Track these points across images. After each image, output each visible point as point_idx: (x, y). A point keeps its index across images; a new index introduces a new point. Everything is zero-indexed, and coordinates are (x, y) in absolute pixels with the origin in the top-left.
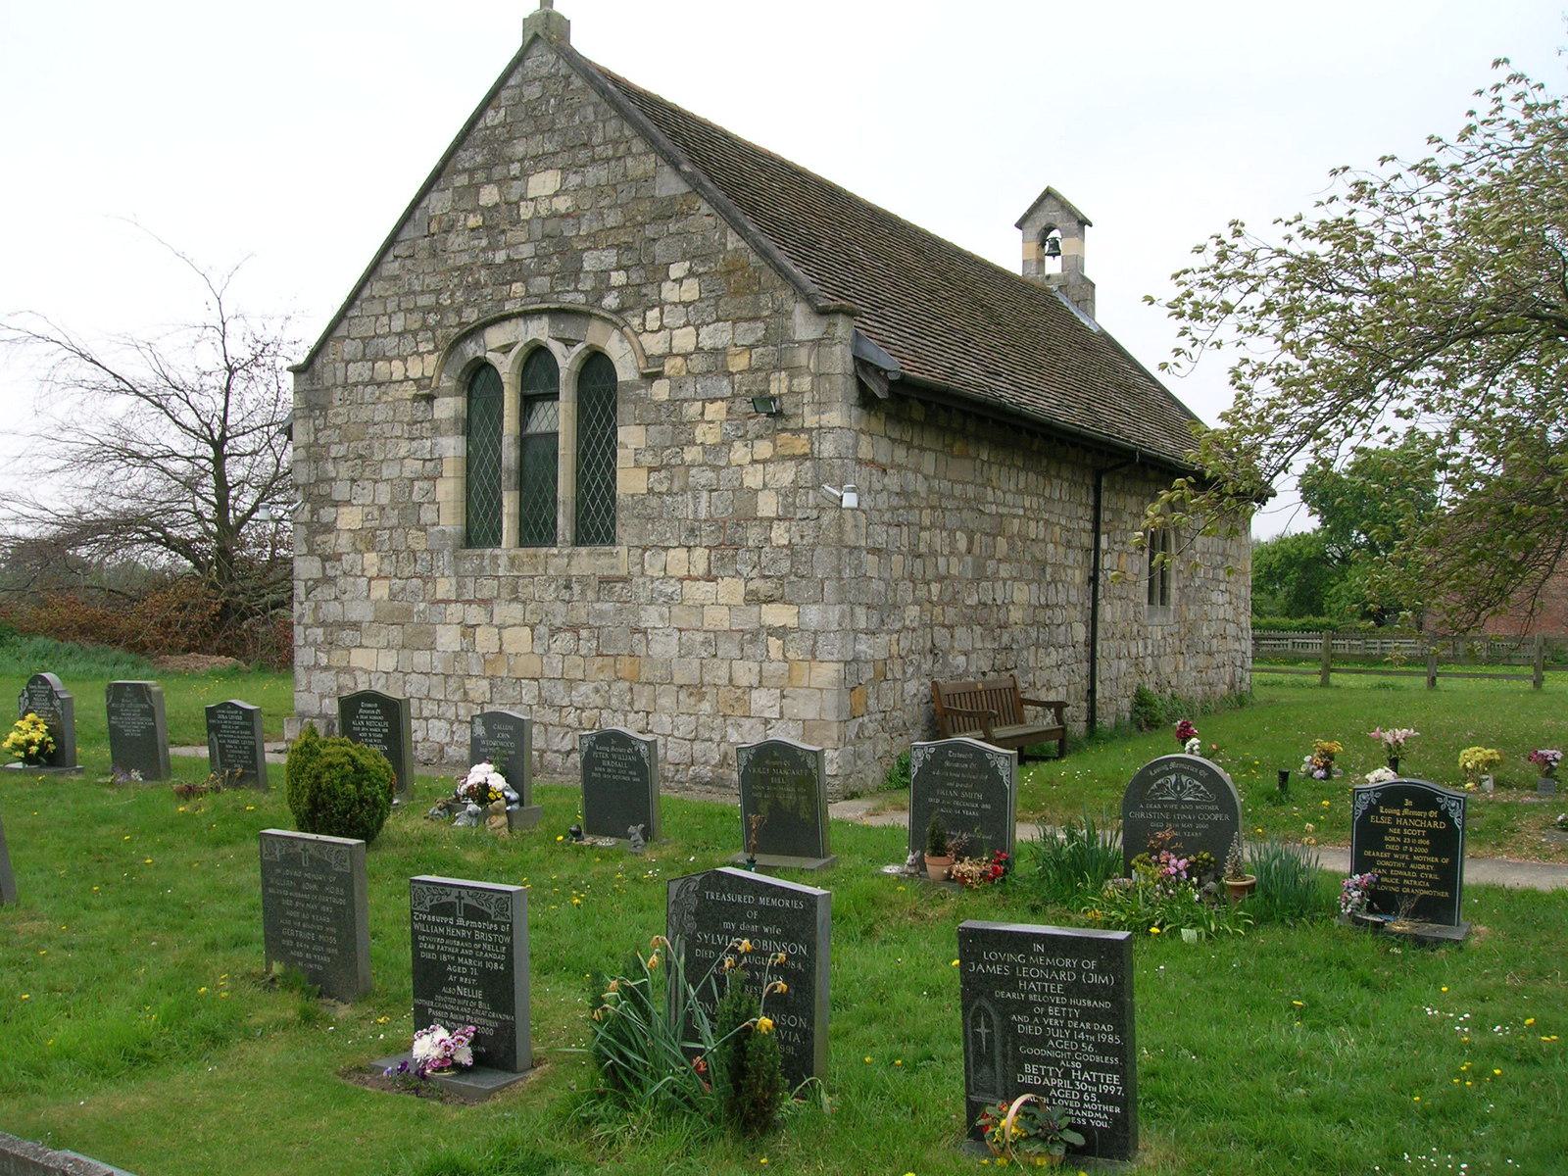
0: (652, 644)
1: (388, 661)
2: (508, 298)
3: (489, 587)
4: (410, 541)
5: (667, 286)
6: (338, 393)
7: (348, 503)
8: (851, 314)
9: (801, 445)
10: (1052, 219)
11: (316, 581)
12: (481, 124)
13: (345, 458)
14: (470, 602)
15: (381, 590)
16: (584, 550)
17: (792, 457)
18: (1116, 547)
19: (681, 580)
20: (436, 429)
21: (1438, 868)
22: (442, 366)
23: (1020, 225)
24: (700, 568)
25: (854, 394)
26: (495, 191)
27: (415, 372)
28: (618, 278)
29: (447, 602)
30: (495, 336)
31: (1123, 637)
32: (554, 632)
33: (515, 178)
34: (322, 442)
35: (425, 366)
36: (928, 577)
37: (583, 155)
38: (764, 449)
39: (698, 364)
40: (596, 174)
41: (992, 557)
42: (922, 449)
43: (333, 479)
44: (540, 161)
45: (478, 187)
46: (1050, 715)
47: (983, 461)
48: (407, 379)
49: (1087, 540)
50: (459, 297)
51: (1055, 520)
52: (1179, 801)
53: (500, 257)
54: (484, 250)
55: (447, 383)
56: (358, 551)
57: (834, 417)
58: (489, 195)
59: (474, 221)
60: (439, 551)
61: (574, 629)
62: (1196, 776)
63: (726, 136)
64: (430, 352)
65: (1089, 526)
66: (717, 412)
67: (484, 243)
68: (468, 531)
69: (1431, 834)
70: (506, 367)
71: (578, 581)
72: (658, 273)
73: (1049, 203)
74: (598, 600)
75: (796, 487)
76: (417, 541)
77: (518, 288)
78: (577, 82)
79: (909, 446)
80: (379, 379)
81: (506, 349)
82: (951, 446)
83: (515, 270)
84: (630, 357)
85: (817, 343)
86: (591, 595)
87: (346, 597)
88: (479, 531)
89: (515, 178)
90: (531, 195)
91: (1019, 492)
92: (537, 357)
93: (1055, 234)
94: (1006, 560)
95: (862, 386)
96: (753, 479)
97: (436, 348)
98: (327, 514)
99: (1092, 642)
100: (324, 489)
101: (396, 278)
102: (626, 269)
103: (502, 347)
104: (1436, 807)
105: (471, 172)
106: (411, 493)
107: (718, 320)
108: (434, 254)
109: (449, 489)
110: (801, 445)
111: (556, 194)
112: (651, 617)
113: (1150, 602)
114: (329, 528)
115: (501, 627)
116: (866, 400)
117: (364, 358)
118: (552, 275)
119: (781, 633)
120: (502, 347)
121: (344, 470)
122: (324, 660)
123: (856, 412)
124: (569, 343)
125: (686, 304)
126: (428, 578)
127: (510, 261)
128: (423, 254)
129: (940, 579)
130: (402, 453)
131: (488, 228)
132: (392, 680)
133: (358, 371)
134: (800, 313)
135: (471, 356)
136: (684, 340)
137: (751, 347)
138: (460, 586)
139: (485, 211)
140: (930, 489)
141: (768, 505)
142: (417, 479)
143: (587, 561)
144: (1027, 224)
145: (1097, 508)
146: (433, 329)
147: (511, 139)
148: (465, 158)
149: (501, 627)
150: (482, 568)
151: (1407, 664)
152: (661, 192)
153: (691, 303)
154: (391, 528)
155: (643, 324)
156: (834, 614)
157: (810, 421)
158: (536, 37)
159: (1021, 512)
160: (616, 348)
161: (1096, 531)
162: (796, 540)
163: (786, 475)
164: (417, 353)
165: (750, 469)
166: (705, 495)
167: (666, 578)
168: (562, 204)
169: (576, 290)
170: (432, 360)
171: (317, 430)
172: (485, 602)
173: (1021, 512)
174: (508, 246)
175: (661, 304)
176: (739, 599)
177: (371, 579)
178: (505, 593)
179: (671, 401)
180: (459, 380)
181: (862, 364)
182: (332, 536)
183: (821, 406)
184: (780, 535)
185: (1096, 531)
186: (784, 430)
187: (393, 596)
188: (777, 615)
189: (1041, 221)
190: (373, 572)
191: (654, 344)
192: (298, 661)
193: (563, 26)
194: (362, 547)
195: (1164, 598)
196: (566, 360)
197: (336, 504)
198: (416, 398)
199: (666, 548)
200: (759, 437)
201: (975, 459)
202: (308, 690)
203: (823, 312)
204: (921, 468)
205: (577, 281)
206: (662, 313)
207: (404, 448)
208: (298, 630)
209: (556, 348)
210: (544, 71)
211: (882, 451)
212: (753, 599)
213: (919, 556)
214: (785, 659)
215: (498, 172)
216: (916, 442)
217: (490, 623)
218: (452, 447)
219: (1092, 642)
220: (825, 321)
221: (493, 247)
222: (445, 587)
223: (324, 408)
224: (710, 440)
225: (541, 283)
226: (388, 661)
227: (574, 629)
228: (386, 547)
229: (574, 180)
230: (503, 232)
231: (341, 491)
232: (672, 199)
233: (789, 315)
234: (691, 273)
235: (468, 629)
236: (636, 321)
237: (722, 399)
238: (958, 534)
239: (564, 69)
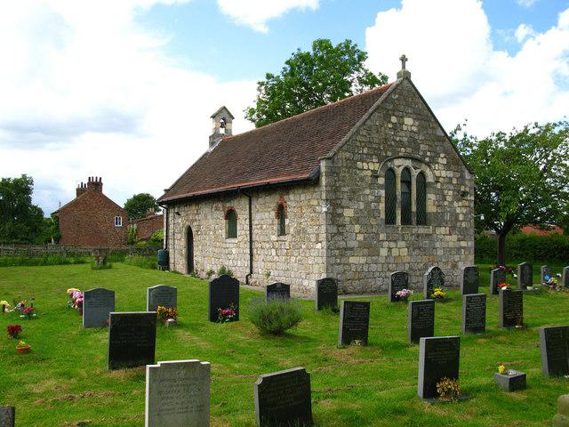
7: (348, 207)
15: (360, 237)
38: (460, 204)
70: (399, 171)
72: (438, 155)
88: (390, 219)
103: (399, 165)
120: (399, 165)
127: (400, 140)
141: (461, 217)
160: (428, 172)
172: (395, 241)
196: (415, 173)
197: (343, 207)
212: (459, 240)
222: (382, 236)
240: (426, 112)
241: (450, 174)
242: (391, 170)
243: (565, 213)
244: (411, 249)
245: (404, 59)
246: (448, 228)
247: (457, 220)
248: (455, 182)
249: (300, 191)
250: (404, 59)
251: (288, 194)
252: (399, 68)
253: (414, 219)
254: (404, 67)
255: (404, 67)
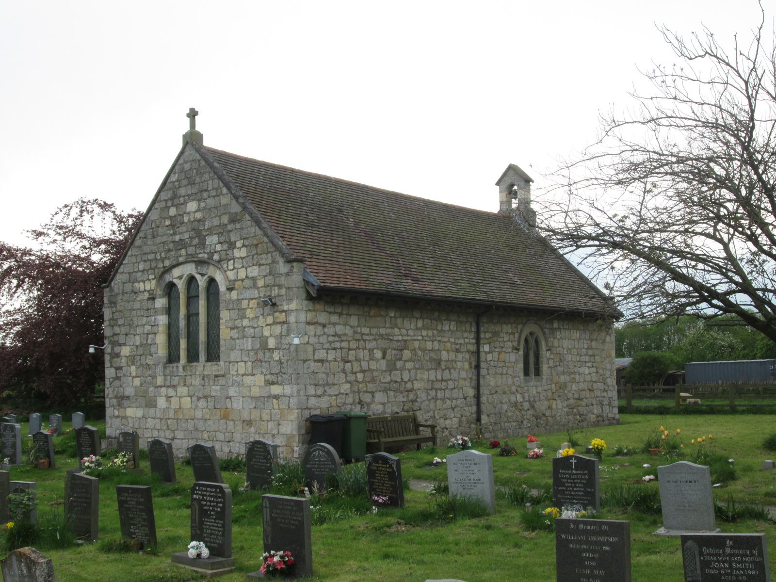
0: (233, 404)
1: (139, 413)
2: (181, 256)
3: (176, 380)
4: (147, 361)
5: (235, 251)
6: (119, 297)
7: (125, 344)
8: (301, 261)
9: (281, 317)
10: (514, 181)
11: (113, 378)
12: (169, 181)
13: (124, 325)
14: (169, 386)
15: (137, 382)
16: (209, 364)
17: (280, 323)
18: (497, 350)
19: (243, 375)
20: (156, 312)
21: (392, 486)
22: (157, 286)
23: (497, 184)
24: (249, 371)
25: (304, 295)
26: (175, 210)
27: (148, 288)
28: (219, 247)
29: (161, 387)
30: (176, 272)
31: (504, 393)
32: (199, 399)
33: (182, 204)
34: (115, 318)
35: (150, 285)
36: (354, 370)
37: (205, 195)
38: (270, 320)
39: (248, 283)
40: (211, 202)
41: (400, 359)
42: (348, 315)
43: (119, 334)
44: (190, 197)
45: (168, 208)
46: (429, 430)
47: (391, 317)
48: (145, 290)
49: (472, 348)
50: (163, 255)
51: (446, 340)
52: (320, 461)
53: (177, 238)
54: (171, 235)
55: (159, 292)
56: (128, 366)
57: (293, 306)
58: (173, 211)
59: (168, 222)
60: (158, 365)
61: (206, 397)
62: (323, 451)
63: (292, 171)
64: (153, 279)
65: (474, 341)
66: (254, 304)
67: (171, 232)
68: (170, 355)
69: (388, 473)
70: (181, 285)
71: (207, 377)
72: (232, 245)
73: (511, 172)
74: (214, 385)
75: (281, 335)
76: (150, 361)
77: (183, 252)
78: (203, 163)
79: (340, 314)
80: (135, 291)
81: (180, 278)
82: (369, 313)
83: (181, 244)
84: (223, 281)
85: (287, 274)
86: (212, 383)
87: (124, 385)
88: (172, 358)
89: (182, 204)
90: (187, 211)
91: (417, 329)
92: (191, 280)
93: (515, 188)
94: (410, 360)
95: (308, 292)
96: (266, 333)
97: (155, 278)
98: (117, 350)
99: (478, 396)
100: (116, 338)
101: (140, 247)
102: (221, 243)
103: (179, 275)
104: (388, 463)
105: (166, 201)
106: (147, 340)
107: (253, 265)
108: (154, 237)
109: (161, 339)
110: (281, 317)
111: (196, 211)
112: (232, 392)
113: (526, 373)
114: (118, 355)
115: (180, 397)
116: (310, 298)
117: (129, 282)
118: (195, 246)
119: (277, 397)
120: (179, 275)
121: (124, 330)
122: (116, 413)
123: (305, 302)
124: (203, 275)
125: (242, 258)
126: (154, 377)
127: (181, 240)
128: (150, 237)
129: (364, 372)
130: (144, 322)
131: (172, 226)
132: (141, 421)
133: (128, 287)
134: (281, 261)
135: (167, 281)
136: (242, 274)
137: (265, 276)
138: (165, 380)
139: (171, 218)
140: (355, 332)
141: (272, 343)
142: (150, 334)
143: (211, 369)
144: (501, 183)
145: (478, 333)
146: (154, 269)
147: (180, 187)
148: (163, 196)
149: (180, 397)
150: (173, 372)
151: (757, 394)
152: (233, 211)
153: (244, 258)
154: (140, 355)
155: (227, 267)
156: (295, 388)
157: (286, 308)
158: (188, 142)
159: (420, 338)
160: (219, 277)
161: (478, 344)
162: (282, 358)
163: (278, 329)
164: (149, 280)
165: (265, 328)
166: (250, 339)
167: (237, 375)
168: (199, 215)
169: (204, 253)
170: (154, 282)
171: (113, 313)
172: (174, 387)
173: (420, 338)
174: (180, 233)
175: (233, 259)
176: (263, 383)
177: (133, 377)
178: (182, 384)
179: (238, 300)
180: (164, 291)
181: (307, 282)
182: (119, 359)
183: (290, 300)
184: (276, 356)
185: (478, 344)
186: (277, 311)
187: (141, 385)
188: (276, 390)
189: (508, 181)
190: (134, 374)
191: (231, 275)
192: (107, 414)
193: (200, 136)
194: (130, 363)
195: (538, 372)
196: (202, 282)
197: (120, 345)
198: (149, 299)
199: (237, 362)
200: (269, 315)
201: (385, 317)
202: (111, 427)
203: (289, 261)
204: (345, 325)
205: (204, 248)
206: (234, 262)
207: (145, 320)
208: (107, 400)
209: (198, 277)
210: (191, 158)
211: (322, 318)
212: (269, 383)
213: (348, 362)
214: (279, 409)
215: (176, 201)
216: (344, 312)
217: (176, 396)
218: (163, 319)
219: (478, 396)
220: (289, 265)
221: (174, 234)
222: (160, 380)
223: (115, 303)
224: (251, 316)
225: (191, 250)
226: (139, 413)
227: (206, 397)
228: (138, 364)
229: (203, 204)
230: (178, 227)
231: (122, 339)
232: (236, 213)
233: (278, 263)
234: (244, 246)
235: (169, 398)
236: (225, 266)
237: (255, 299)
238: (375, 351)
239: (199, 157)
240: (177, 167)
241: (254, 271)
242: (171, 286)
243: (92, 350)
244: (194, 398)
245: (193, 114)
246: (249, 364)
247: (264, 346)
248: (261, 283)
249: (417, 315)
250: (193, 114)
251: (404, 318)
252: (186, 128)
253: (202, 356)
254: (193, 124)
255: (193, 124)
